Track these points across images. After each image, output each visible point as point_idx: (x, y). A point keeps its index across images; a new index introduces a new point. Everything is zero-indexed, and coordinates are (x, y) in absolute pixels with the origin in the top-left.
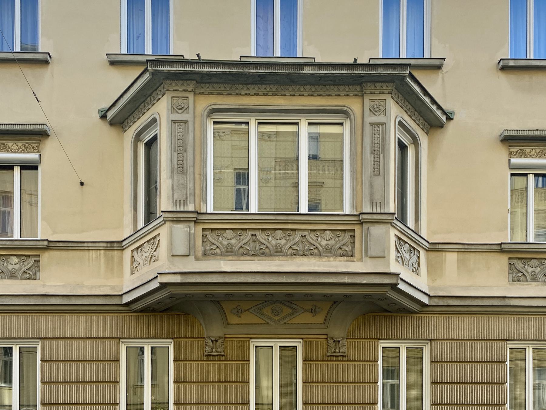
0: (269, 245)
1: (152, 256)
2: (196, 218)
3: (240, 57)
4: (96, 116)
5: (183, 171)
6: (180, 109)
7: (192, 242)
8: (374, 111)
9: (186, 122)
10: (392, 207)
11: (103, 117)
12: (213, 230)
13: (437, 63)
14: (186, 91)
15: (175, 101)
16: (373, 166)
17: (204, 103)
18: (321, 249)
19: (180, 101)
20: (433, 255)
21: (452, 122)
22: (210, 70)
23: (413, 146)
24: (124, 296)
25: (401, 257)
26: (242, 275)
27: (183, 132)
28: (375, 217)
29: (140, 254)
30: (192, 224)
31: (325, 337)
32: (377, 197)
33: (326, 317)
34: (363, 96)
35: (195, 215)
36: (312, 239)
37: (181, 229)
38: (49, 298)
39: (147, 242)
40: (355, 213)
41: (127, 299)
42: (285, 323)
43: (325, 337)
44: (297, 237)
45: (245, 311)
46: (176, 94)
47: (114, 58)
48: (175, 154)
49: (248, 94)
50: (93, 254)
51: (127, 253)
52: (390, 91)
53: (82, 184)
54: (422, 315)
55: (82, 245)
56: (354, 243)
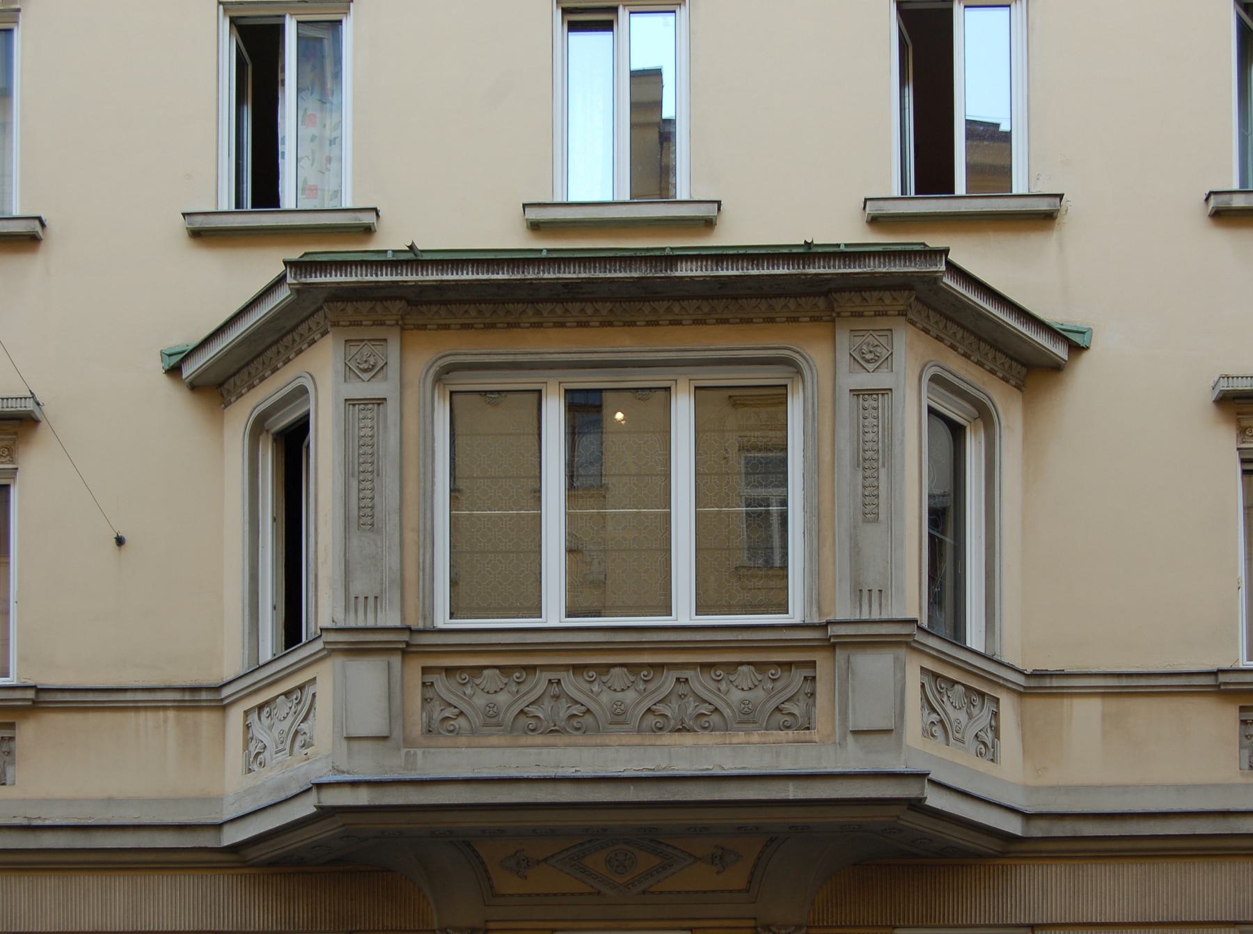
0: (592, 706)
1: (297, 732)
2: (408, 644)
3: (525, 206)
4: (156, 368)
5: (372, 525)
6: (365, 371)
7: (397, 701)
8: (862, 360)
9: (381, 401)
10: (910, 599)
11: (174, 371)
12: (449, 670)
13: (1043, 205)
14: (382, 323)
15: (354, 350)
16: (860, 499)
17: (422, 359)
18: (727, 712)
19: (366, 350)
20: (1036, 705)
21: (1086, 356)
22: (440, 277)
23: (980, 423)
24: (226, 829)
25: (941, 721)
26: (523, 785)
27: (372, 428)
28: (866, 630)
29: (266, 722)
30: (396, 660)
31: (752, 923)
32: (871, 579)
33: (752, 874)
34: (833, 321)
35: (405, 637)
36: (705, 688)
37: (369, 676)
38: (38, 833)
39: (287, 694)
40: (816, 621)
41: (232, 836)
42: (644, 892)
43: (752, 923)
44: (668, 681)
45: (538, 862)
46: (355, 333)
47: (200, 222)
48: (354, 483)
49: (539, 325)
50: (148, 720)
51: (235, 716)
52: (902, 308)
53: (120, 541)
54: (1009, 862)
55: (121, 697)
56: (813, 694)
